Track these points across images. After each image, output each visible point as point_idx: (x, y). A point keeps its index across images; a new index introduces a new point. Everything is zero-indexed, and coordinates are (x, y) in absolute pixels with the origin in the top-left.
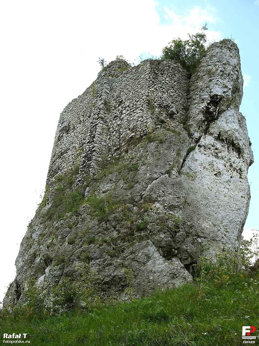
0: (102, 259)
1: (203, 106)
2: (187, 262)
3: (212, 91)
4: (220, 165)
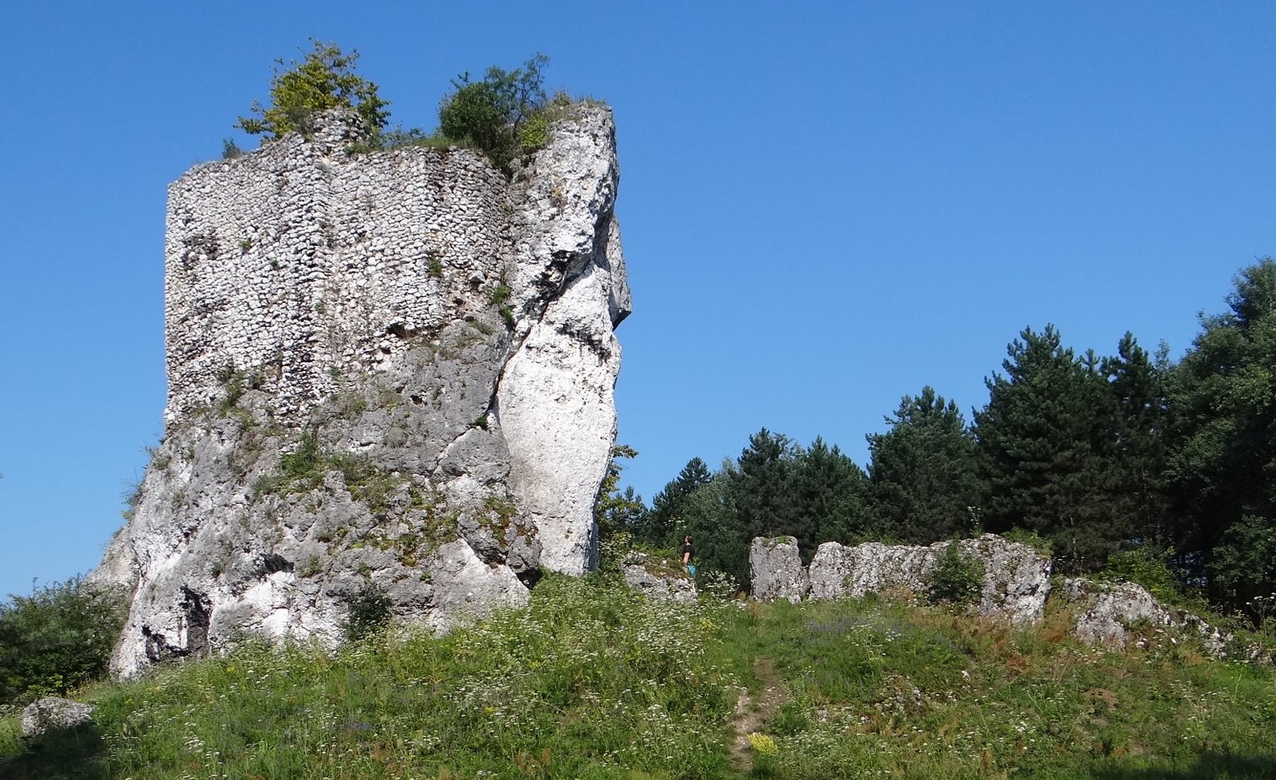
0: (390, 569)
1: (537, 273)
2: (520, 571)
3: (555, 242)
4: (563, 381)
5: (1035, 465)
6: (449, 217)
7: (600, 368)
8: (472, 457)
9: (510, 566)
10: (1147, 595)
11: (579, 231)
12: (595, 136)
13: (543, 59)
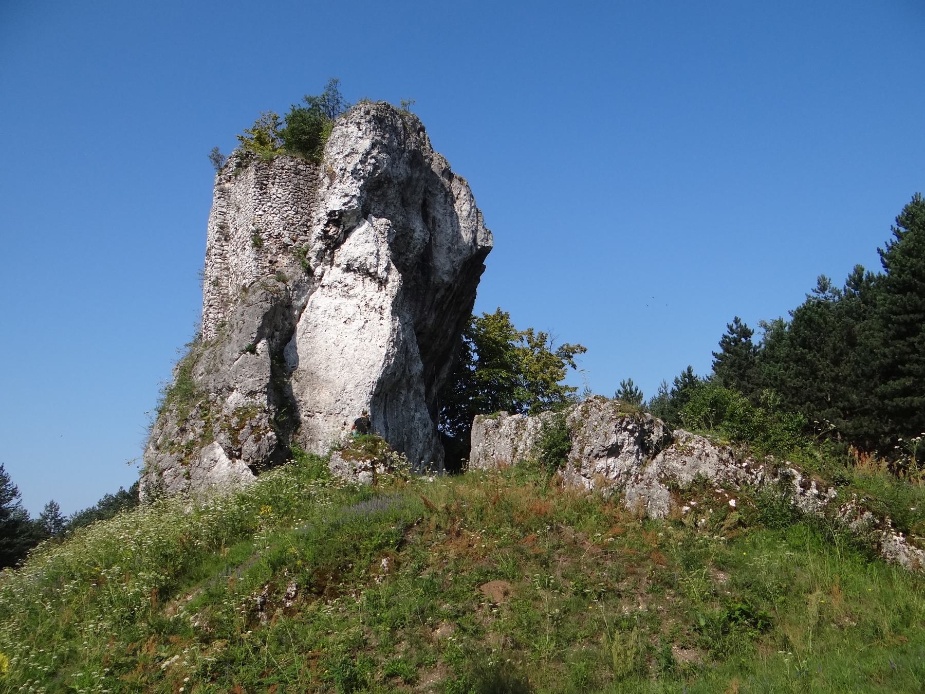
4: (349, 307)
5: (906, 317)
6: (269, 204)
7: (379, 293)
8: (238, 376)
9: (244, 460)
10: (709, 448)
11: (343, 194)
12: (359, 124)
13: (336, 82)
